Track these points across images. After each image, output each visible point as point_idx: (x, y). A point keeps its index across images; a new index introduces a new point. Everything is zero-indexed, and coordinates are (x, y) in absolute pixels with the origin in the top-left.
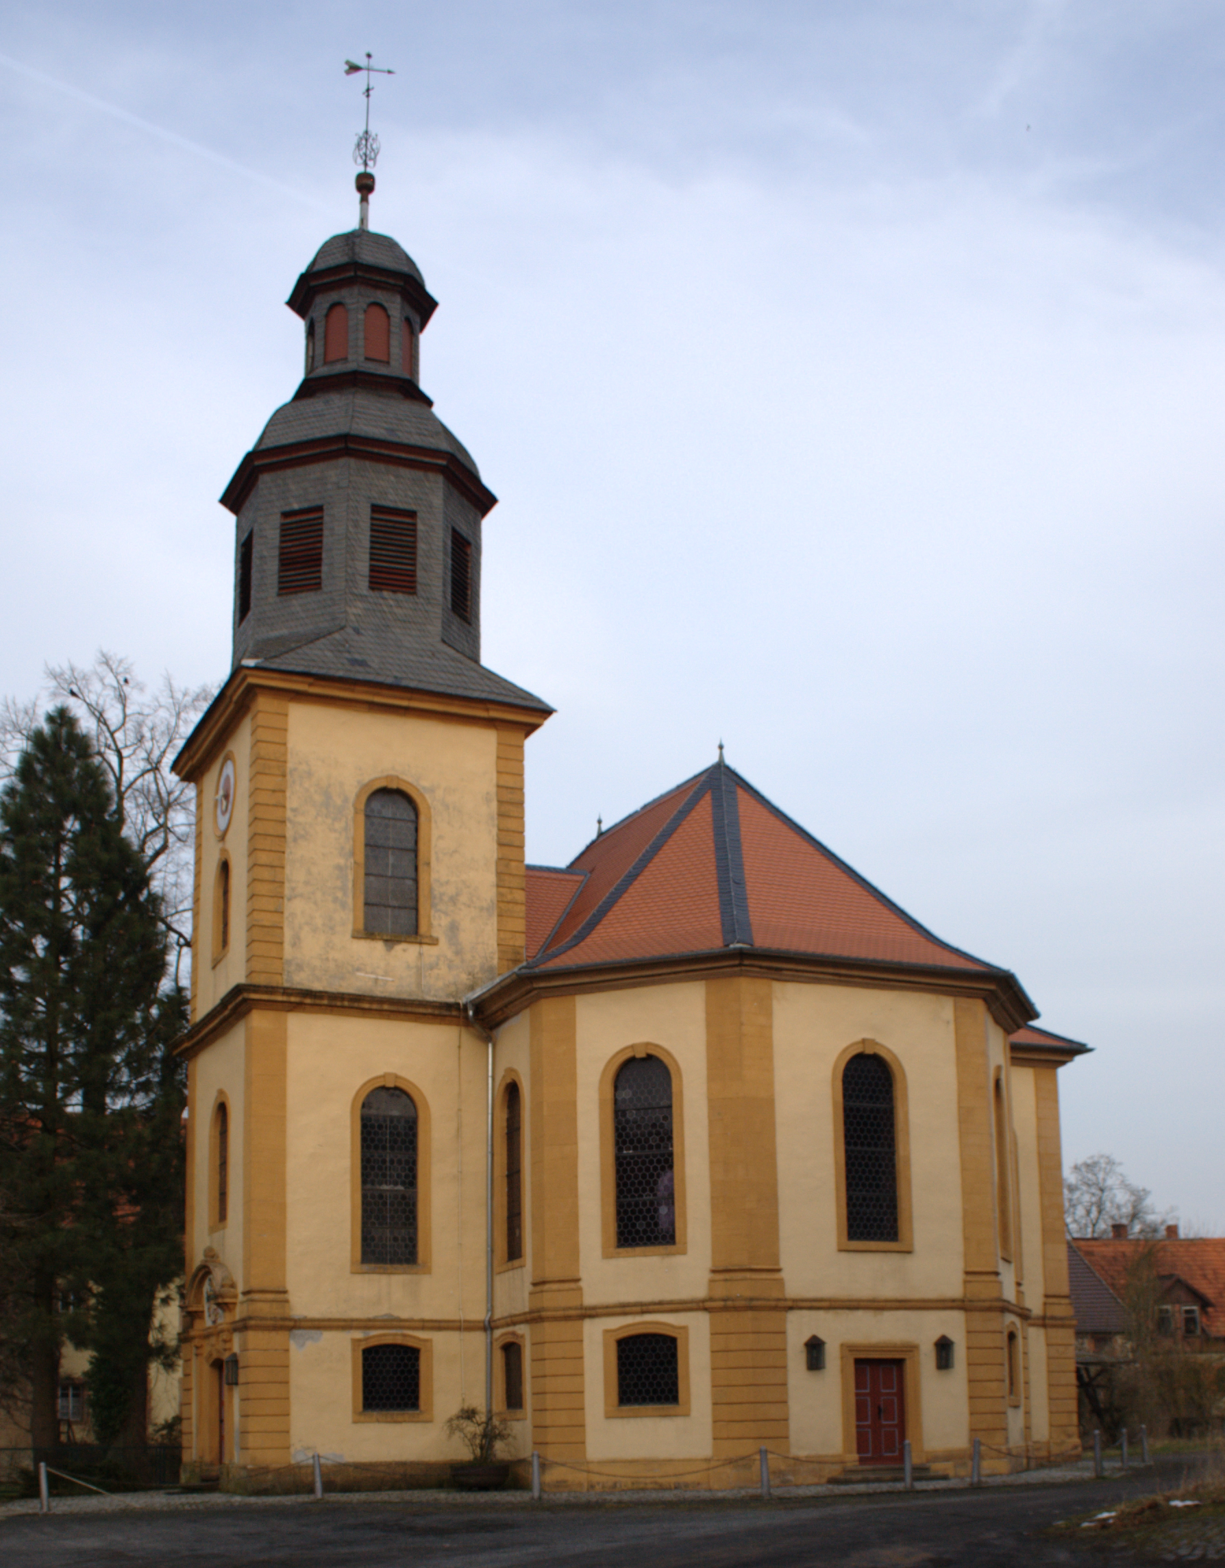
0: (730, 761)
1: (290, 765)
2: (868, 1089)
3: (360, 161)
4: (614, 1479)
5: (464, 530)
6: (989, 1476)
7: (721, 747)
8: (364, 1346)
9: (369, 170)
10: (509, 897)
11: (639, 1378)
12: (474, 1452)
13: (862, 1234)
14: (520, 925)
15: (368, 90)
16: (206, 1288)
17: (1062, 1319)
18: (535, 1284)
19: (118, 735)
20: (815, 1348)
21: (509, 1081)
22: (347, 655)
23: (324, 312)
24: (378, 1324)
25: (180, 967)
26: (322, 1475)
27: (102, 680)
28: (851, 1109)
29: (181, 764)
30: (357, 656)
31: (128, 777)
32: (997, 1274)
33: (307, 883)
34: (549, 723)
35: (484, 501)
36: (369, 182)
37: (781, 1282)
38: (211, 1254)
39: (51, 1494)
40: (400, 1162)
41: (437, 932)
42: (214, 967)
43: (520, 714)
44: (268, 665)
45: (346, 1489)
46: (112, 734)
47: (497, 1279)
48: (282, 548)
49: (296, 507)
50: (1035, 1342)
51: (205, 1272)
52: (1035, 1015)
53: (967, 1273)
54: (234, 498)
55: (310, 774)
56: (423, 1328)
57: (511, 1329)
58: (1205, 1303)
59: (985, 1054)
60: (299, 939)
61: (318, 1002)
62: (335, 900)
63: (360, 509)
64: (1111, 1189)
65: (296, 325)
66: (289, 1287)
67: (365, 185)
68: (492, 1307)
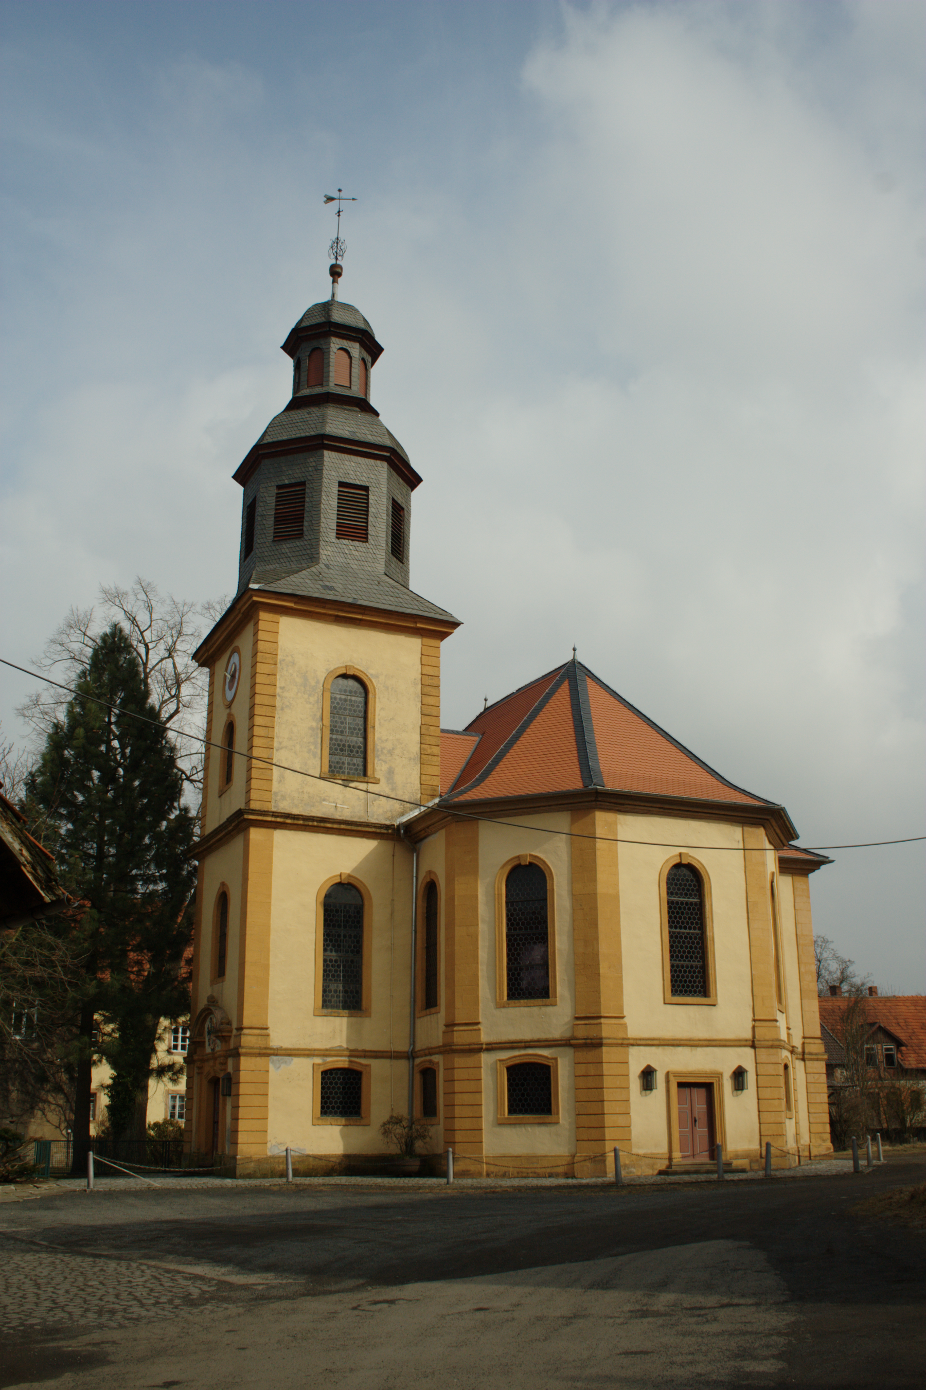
0: (580, 658)
1: (280, 657)
2: (686, 891)
3: (333, 257)
4: (506, 1169)
5: (400, 500)
6: (776, 1170)
7: (574, 650)
8: (322, 1068)
9: (338, 262)
10: (429, 751)
11: (523, 1095)
12: (401, 1149)
13: (681, 991)
14: (436, 771)
15: (339, 212)
16: (207, 1024)
17: (816, 1054)
18: (446, 1026)
19: (147, 635)
20: (648, 1075)
21: (428, 880)
22: (321, 583)
23: (308, 354)
24: (333, 1053)
25: (190, 797)
26: (293, 1163)
27: (136, 595)
28: (672, 902)
29: (200, 654)
30: (328, 584)
31: (153, 660)
32: (776, 1021)
33: (290, 739)
34: (457, 631)
35: (412, 480)
36: (339, 270)
37: (625, 1026)
38: (212, 1001)
39: (96, 1175)
40: (350, 936)
41: (378, 775)
42: (220, 797)
43: (434, 626)
44: (267, 588)
45: (307, 1174)
46: (142, 633)
47: (418, 1021)
48: (276, 510)
49: (287, 482)
50: (798, 1070)
51: (208, 1012)
52: (797, 837)
53: (577, 1018)
54: (242, 476)
55: (293, 663)
56: (365, 1057)
57: (428, 1058)
58: (899, 1043)
59: (764, 864)
60: (283, 778)
61: (296, 822)
62: (309, 751)
63: (317, 483)
64: (826, 960)
65: (288, 363)
66: (269, 1025)
67: (335, 272)
68: (414, 1042)
